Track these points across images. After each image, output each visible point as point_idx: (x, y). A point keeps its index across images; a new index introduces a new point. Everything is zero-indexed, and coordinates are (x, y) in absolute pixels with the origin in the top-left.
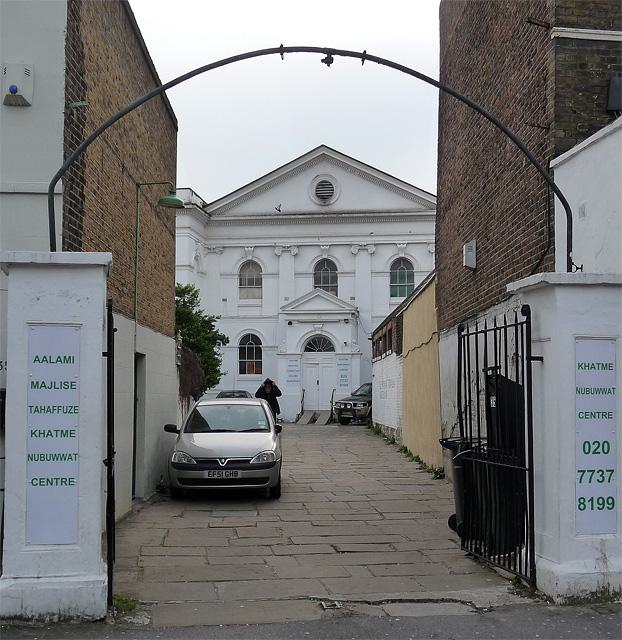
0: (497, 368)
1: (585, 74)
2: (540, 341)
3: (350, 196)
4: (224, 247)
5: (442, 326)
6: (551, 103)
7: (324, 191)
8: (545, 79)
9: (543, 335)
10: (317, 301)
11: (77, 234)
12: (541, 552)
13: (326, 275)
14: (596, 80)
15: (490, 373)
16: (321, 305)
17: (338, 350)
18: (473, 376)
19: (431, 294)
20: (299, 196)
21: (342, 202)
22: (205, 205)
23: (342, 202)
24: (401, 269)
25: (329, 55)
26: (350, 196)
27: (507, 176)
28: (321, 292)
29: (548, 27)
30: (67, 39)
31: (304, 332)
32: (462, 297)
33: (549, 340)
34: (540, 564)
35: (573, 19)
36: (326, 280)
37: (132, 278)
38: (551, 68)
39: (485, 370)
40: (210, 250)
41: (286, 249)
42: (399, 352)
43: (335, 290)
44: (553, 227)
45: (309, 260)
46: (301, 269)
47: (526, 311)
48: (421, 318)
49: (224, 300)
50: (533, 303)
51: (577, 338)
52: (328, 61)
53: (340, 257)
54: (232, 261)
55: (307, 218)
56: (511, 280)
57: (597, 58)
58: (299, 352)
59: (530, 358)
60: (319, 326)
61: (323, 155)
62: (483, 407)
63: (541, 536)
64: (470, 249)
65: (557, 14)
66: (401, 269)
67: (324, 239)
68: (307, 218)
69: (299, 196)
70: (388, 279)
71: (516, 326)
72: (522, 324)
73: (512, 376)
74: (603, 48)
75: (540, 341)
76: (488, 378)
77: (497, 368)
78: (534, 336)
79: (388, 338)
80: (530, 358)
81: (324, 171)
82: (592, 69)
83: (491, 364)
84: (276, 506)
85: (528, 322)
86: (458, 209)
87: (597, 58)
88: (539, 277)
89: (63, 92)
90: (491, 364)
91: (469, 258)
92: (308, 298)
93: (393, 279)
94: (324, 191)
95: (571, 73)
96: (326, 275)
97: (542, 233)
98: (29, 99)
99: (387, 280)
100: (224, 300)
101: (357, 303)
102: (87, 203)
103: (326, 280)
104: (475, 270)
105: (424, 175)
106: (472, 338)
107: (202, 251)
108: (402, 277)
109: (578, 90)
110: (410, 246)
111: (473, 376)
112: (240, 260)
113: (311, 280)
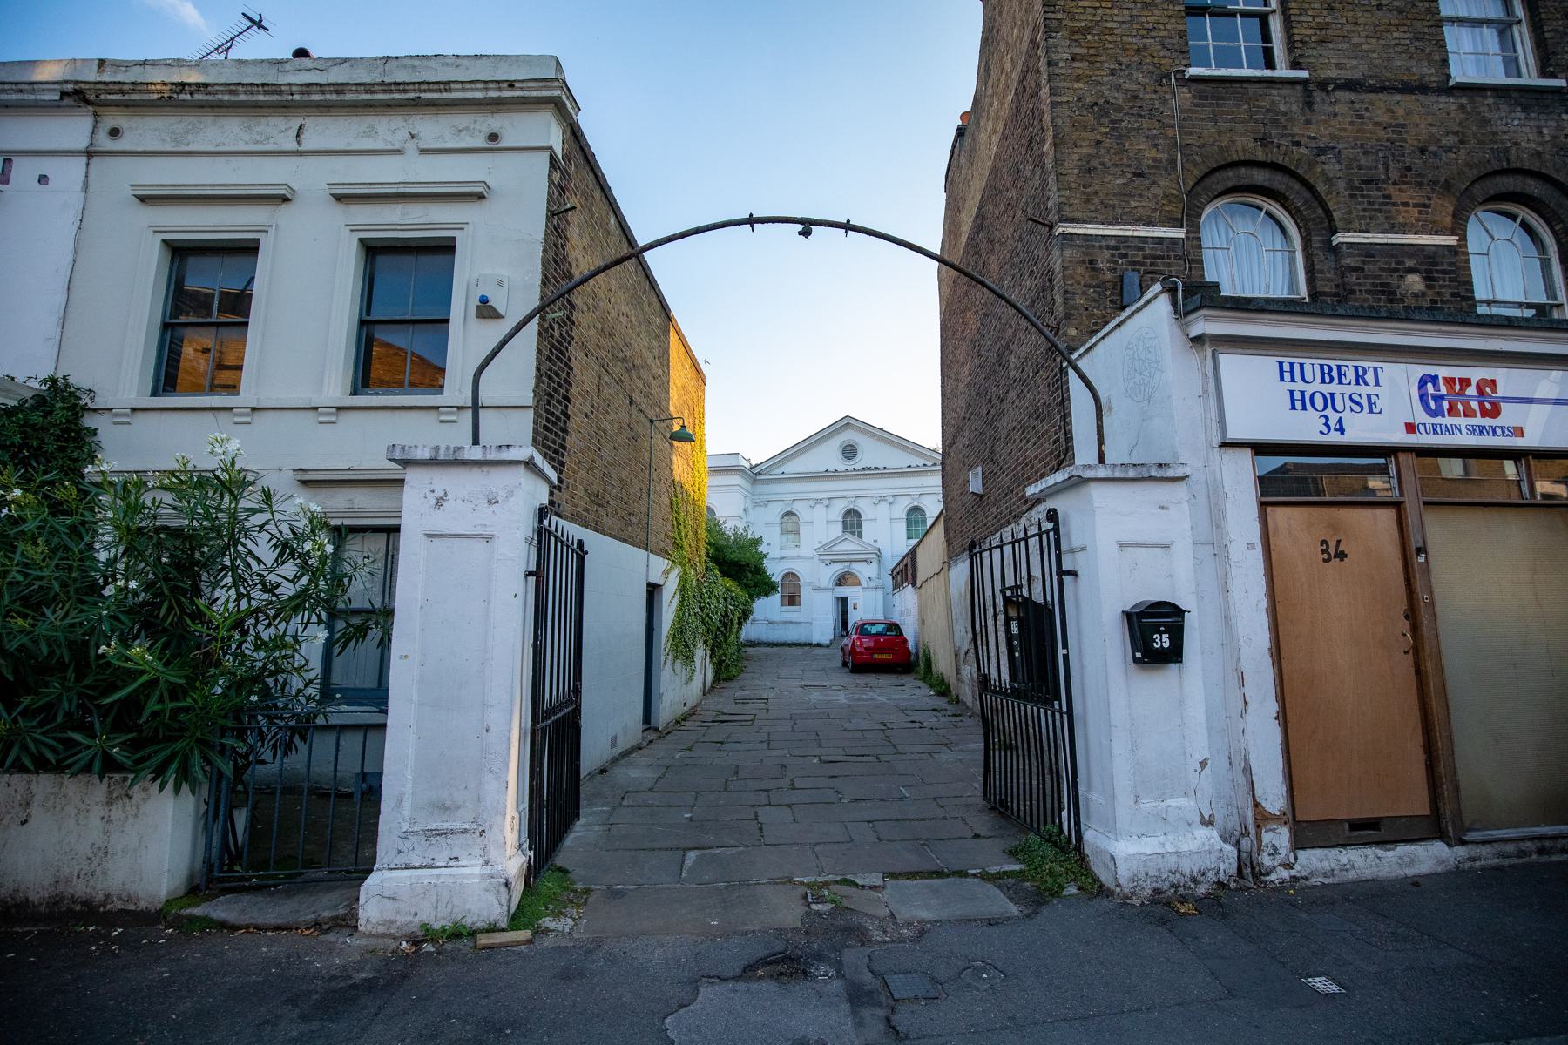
0: (1018, 587)
1: (1094, 269)
2: (1072, 551)
3: (870, 454)
5: (951, 557)
6: (1059, 300)
7: (849, 452)
8: (1050, 280)
9: (1076, 543)
11: (556, 452)
12: (1088, 818)
13: (852, 521)
14: (1108, 276)
15: (1009, 593)
16: (850, 545)
17: (864, 584)
18: (989, 602)
19: (940, 529)
20: (829, 457)
21: (865, 459)
23: (865, 459)
24: (915, 513)
25: (807, 227)
26: (870, 454)
27: (1012, 395)
28: (848, 536)
29: (1051, 227)
30: (545, 250)
31: (838, 568)
32: (971, 524)
33: (1084, 549)
34: (1088, 836)
35: (1078, 215)
36: (852, 526)
37: (644, 509)
38: (1058, 267)
39: (1003, 591)
40: (756, 504)
41: (818, 501)
42: (914, 584)
43: (860, 536)
44: (1070, 431)
45: (839, 508)
46: (831, 518)
47: (1052, 515)
48: (932, 554)
50: (1059, 503)
51: (1121, 546)
52: (806, 233)
53: (863, 506)
54: (775, 511)
55: (836, 475)
56: (1173, 241)
57: (1107, 254)
59: (1061, 573)
61: (847, 423)
62: (1002, 634)
63: (1088, 800)
64: (975, 475)
65: (1060, 210)
66: (915, 513)
67: (848, 492)
68: (836, 475)
69: (829, 457)
71: (1040, 535)
72: (1047, 532)
73: (1037, 596)
74: (1113, 243)
75: (1072, 551)
76: (1007, 601)
77: (1018, 587)
78: (1064, 547)
79: (906, 572)
80: (1061, 573)
81: (848, 436)
82: (1102, 264)
83: (1010, 582)
85: (1056, 530)
86: (962, 442)
87: (1107, 254)
88: (1059, 477)
90: (1010, 582)
91: (975, 484)
92: (836, 541)
93: (909, 523)
94: (849, 452)
95: (1080, 270)
96: (852, 521)
97: (1057, 440)
98: (501, 311)
99: (904, 525)
101: (878, 545)
102: (572, 425)
103: (852, 526)
104: (981, 497)
105: (930, 434)
106: (986, 554)
107: (749, 505)
108: (916, 522)
109: (1087, 286)
111: (989, 602)
113: (840, 527)
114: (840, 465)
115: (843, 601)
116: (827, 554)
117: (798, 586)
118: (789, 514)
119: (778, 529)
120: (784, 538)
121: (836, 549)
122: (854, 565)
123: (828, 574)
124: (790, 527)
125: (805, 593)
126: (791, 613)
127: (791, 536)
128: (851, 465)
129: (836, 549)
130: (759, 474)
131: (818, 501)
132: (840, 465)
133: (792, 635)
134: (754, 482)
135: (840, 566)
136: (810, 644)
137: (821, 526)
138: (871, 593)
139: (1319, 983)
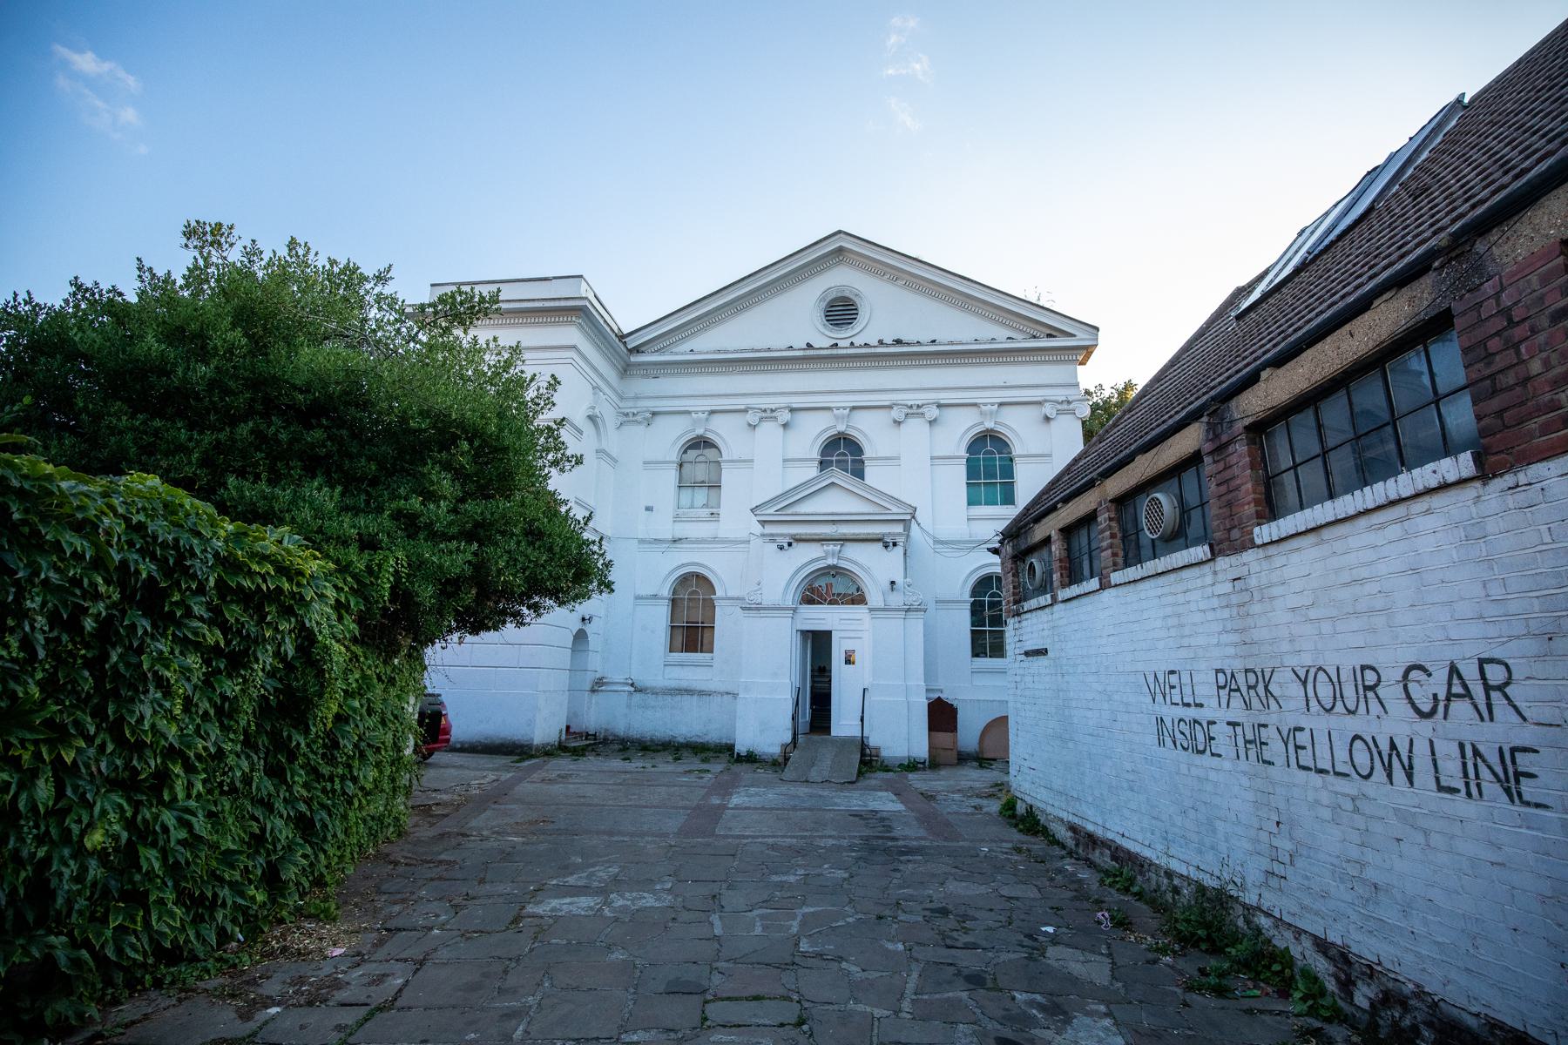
3: (887, 315)
4: (654, 414)
7: (841, 311)
10: (833, 494)
17: (874, 598)
20: (795, 320)
21: (872, 328)
22: (622, 337)
23: (872, 328)
26: (887, 315)
28: (838, 476)
31: (808, 557)
40: (627, 418)
43: (859, 473)
49: (649, 509)
55: (809, 359)
58: (789, 603)
60: (831, 547)
61: (837, 250)
68: (809, 359)
70: (963, 470)
81: (840, 279)
84: (1061, 525)
89: (788, 723)
94: (841, 311)
99: (962, 471)
100: (649, 509)
106: (1289, 478)
110: (1006, 409)
112: (679, 438)
114: (822, 337)
115: (818, 644)
116: (782, 522)
117: (710, 606)
118: (701, 443)
119: (671, 475)
120: (686, 495)
121: (807, 508)
122: (852, 551)
123: (782, 572)
124: (700, 472)
125: (726, 622)
126: (691, 670)
127: (701, 496)
128: (843, 336)
129: (807, 508)
130: (637, 350)
131: (768, 414)
132: (822, 337)
133: (688, 722)
134: (626, 370)
135: (814, 551)
136: (725, 750)
137: (769, 462)
138: (893, 626)
139: (1050, 930)
